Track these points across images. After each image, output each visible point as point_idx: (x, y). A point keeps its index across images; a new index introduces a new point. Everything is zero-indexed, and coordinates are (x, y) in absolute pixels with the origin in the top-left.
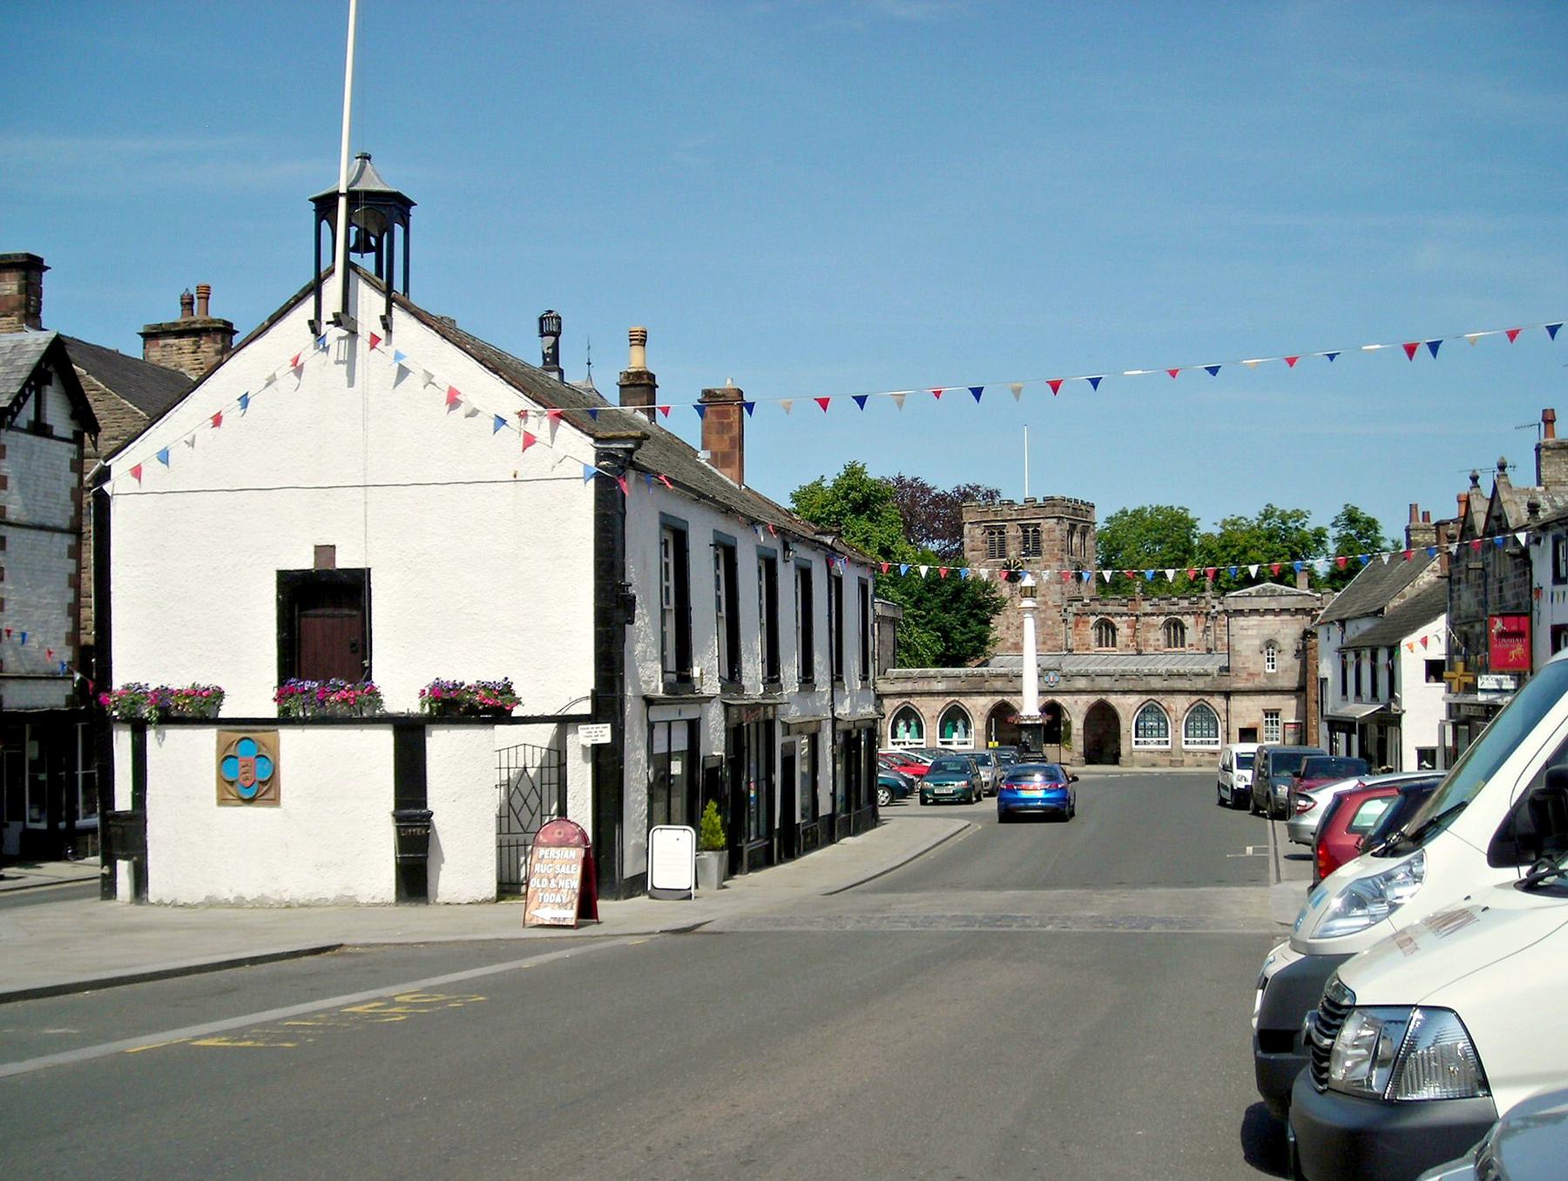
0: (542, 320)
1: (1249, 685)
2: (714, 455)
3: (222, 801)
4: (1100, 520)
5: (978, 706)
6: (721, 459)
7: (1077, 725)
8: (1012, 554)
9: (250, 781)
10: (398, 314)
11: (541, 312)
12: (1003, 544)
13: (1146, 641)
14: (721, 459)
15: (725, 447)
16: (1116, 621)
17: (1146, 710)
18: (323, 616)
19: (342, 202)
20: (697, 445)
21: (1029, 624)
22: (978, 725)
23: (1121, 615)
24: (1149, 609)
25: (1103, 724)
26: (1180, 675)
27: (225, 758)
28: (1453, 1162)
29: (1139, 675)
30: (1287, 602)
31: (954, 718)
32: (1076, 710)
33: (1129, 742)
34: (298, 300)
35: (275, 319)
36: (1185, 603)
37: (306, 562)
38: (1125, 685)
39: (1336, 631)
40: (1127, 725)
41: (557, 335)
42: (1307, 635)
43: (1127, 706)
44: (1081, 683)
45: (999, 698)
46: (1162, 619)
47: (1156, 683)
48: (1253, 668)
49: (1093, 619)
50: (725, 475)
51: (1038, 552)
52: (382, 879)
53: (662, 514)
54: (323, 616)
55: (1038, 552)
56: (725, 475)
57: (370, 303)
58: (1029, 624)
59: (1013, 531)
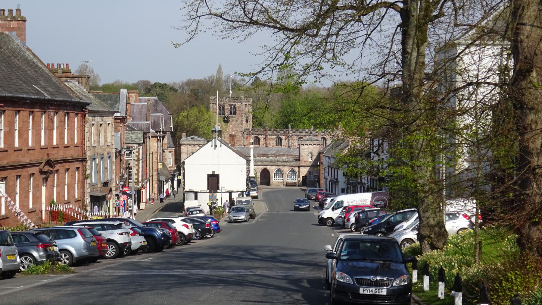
1: (305, 164)
8: (226, 114)
12: (224, 110)
13: (269, 143)
17: (279, 170)
18: (213, 181)
20: (228, 142)
21: (252, 150)
23: (261, 135)
24: (271, 134)
26: (286, 162)
27: (210, 196)
28: (354, 237)
36: (282, 132)
38: (271, 164)
43: (272, 170)
46: (275, 137)
47: (280, 164)
49: (253, 136)
57: (218, 143)
58: (252, 150)
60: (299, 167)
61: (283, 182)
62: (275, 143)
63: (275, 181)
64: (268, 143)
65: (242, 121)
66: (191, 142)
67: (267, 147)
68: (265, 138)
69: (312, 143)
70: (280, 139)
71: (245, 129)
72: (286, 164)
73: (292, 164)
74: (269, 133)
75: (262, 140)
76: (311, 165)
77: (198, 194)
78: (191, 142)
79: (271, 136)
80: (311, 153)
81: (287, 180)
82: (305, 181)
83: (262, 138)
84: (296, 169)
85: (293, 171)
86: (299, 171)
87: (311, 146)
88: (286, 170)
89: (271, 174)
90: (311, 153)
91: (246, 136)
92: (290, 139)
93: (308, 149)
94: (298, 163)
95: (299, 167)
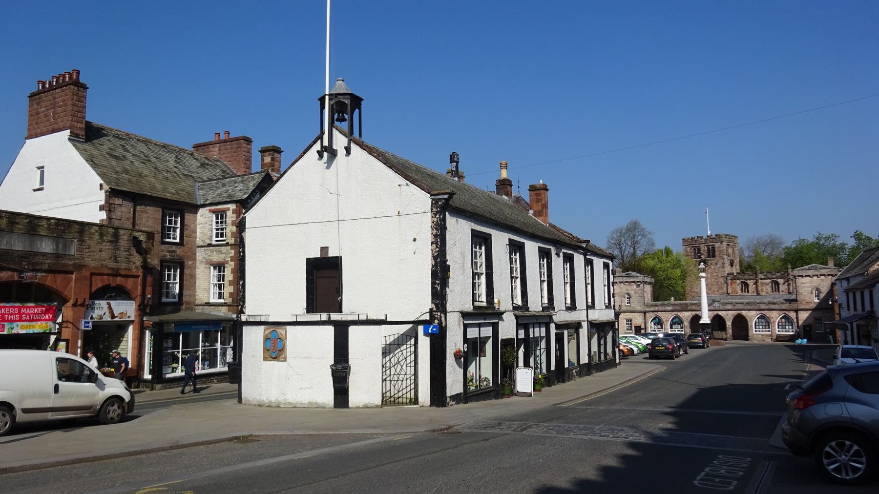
0: (451, 156)
1: (807, 307)
2: (535, 212)
3: (265, 359)
4: (741, 242)
5: (686, 316)
6: (538, 214)
7: (729, 324)
8: (703, 257)
9: (275, 350)
10: (353, 146)
11: (451, 153)
14: (538, 214)
15: (540, 208)
16: (748, 282)
17: (762, 317)
18: (324, 278)
19: (327, 97)
21: (703, 281)
22: (686, 324)
25: (741, 324)
26: (774, 303)
27: (266, 339)
29: (755, 303)
30: (824, 271)
31: (676, 321)
32: (729, 317)
33: (753, 331)
34: (315, 142)
35: (305, 152)
37: (317, 255)
38: (749, 307)
39: (845, 284)
40: (752, 324)
41: (457, 162)
42: (833, 285)
43: (752, 317)
44: (729, 307)
45: (694, 313)
46: (768, 281)
47: (763, 306)
48: (807, 299)
49: (738, 281)
50: (539, 220)
51: (714, 256)
52: (326, 395)
53: (472, 230)
54: (324, 278)
55: (714, 256)
56: (539, 220)
57: (340, 141)
58: (703, 281)
59: (704, 248)
60: (796, 311)
61: (771, 335)
62: (770, 289)
63: (757, 333)
64: (760, 289)
65: (723, 264)
66: (625, 280)
67: (758, 294)
68: (756, 283)
69: (817, 273)
70: (777, 284)
71: (729, 274)
72: (773, 307)
73: (784, 307)
74: (761, 276)
75: (752, 287)
76: (813, 306)
77: (352, 330)
78: (625, 280)
79: (763, 281)
80: (817, 289)
81: (777, 331)
82: (806, 330)
83: (751, 283)
84: (792, 315)
85: (786, 318)
86: (797, 318)
87: (815, 278)
88: (775, 317)
89: (749, 323)
90: (817, 289)
91: (729, 281)
92: (790, 282)
93: (810, 282)
94: (794, 306)
95: (796, 311)
